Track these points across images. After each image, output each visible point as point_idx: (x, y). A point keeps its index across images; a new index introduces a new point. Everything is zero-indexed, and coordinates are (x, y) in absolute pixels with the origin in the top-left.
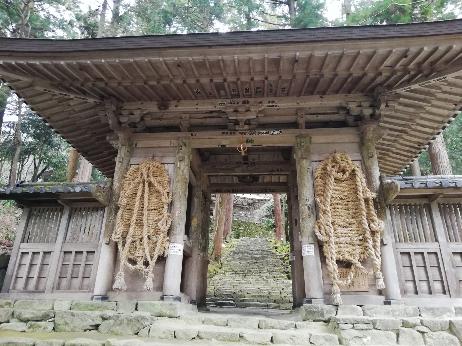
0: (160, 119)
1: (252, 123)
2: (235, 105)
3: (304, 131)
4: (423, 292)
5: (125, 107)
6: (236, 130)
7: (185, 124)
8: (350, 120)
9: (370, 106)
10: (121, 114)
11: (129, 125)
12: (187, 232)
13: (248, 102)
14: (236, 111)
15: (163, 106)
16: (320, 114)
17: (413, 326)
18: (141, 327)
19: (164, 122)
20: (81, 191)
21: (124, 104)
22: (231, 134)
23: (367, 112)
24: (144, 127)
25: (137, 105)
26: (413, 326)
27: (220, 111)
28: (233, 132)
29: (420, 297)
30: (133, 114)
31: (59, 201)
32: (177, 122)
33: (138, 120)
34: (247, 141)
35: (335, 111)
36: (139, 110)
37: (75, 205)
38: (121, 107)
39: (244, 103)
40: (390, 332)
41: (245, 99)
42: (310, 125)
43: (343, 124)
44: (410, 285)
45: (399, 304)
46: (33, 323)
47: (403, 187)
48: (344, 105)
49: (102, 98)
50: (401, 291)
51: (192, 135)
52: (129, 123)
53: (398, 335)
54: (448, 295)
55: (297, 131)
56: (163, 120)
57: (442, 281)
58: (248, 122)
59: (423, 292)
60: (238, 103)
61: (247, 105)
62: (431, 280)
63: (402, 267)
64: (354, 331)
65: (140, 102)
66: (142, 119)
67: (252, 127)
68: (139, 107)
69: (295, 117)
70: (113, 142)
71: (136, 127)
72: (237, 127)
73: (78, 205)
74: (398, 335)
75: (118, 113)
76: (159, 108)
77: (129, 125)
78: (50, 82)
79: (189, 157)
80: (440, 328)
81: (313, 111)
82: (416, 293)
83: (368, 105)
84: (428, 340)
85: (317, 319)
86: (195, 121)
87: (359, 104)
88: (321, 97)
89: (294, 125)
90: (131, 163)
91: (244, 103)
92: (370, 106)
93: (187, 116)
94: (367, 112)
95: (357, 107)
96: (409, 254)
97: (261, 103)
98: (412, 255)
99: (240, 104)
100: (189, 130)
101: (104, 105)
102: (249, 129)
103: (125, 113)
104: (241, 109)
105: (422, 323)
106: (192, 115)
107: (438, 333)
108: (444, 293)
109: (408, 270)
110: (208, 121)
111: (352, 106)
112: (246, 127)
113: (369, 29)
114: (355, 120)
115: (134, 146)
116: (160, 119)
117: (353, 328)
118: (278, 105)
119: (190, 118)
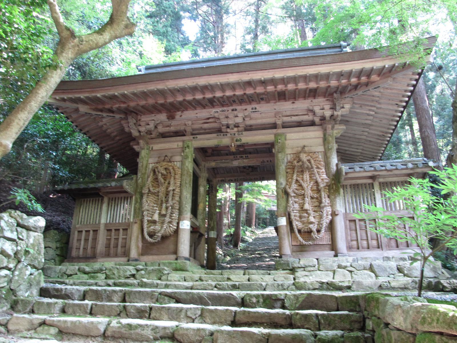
0: (169, 126)
1: (240, 126)
2: (226, 113)
3: (281, 131)
4: (363, 248)
5: (143, 119)
6: (227, 132)
7: (189, 129)
8: (317, 120)
9: (331, 109)
10: (140, 125)
11: (146, 133)
12: (194, 212)
13: (236, 110)
14: (227, 117)
15: (171, 117)
16: (294, 116)
17: (345, 268)
18: (162, 275)
19: (172, 129)
20: (116, 186)
21: (142, 116)
22: (224, 135)
23: (328, 113)
24: (158, 134)
25: (152, 117)
26: (345, 268)
27: (214, 117)
28: (225, 134)
29: (361, 251)
30: (149, 125)
31: (100, 194)
32: (182, 128)
33: (153, 129)
34: (237, 141)
35: (306, 113)
36: (153, 121)
37: (111, 196)
38: (140, 120)
39: (233, 110)
40: (329, 272)
41: (234, 107)
42: (285, 126)
43: (312, 124)
44: (354, 243)
45: (344, 256)
46: (92, 274)
47: (347, 171)
48: (311, 108)
49: (126, 114)
50: (347, 247)
51: (194, 138)
52: (146, 131)
53: (334, 274)
54: (381, 249)
55: (274, 131)
56: (172, 128)
57: (377, 240)
58: (237, 126)
59: (363, 248)
60: (228, 111)
61: (235, 112)
62: (369, 239)
63: (349, 231)
64: (304, 272)
65: (153, 115)
66: (156, 127)
67: (240, 129)
68: (153, 118)
69: (274, 119)
70: (135, 147)
71: (151, 134)
72: (228, 130)
73: (114, 196)
74: (334, 274)
75: (137, 124)
76: (168, 118)
77: (146, 133)
78: (89, 107)
79: (192, 155)
80: (363, 268)
81: (288, 113)
82: (358, 248)
83: (329, 108)
84: (353, 275)
85: (285, 268)
86: (196, 126)
87: (322, 107)
88: (293, 103)
89: (274, 126)
90: (149, 162)
91: (233, 110)
92: (331, 109)
93: (190, 123)
94: (328, 113)
95: (321, 109)
96: (355, 221)
97: (246, 109)
98: (357, 221)
99: (230, 111)
100: (192, 134)
101: (127, 119)
102: (238, 131)
103: (142, 124)
104: (231, 116)
105: (351, 266)
106: (194, 122)
107: (361, 271)
108: (379, 248)
109: (354, 232)
110: (206, 126)
111: (317, 109)
112: (236, 129)
113: (311, 58)
114: (321, 120)
115: (151, 149)
116: (169, 126)
117: (304, 270)
118: (259, 110)
119: (192, 124)
